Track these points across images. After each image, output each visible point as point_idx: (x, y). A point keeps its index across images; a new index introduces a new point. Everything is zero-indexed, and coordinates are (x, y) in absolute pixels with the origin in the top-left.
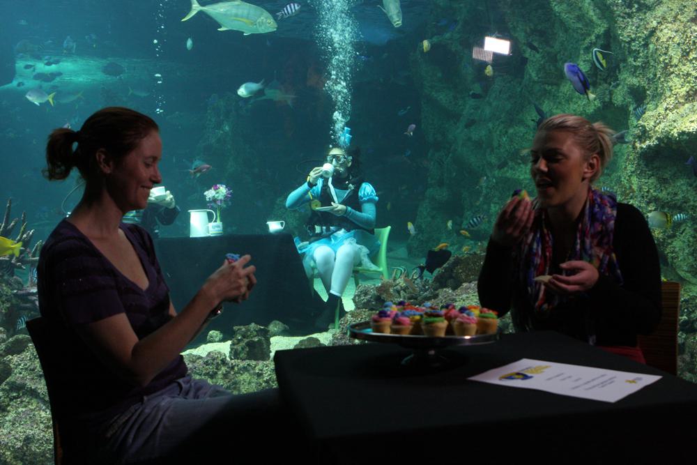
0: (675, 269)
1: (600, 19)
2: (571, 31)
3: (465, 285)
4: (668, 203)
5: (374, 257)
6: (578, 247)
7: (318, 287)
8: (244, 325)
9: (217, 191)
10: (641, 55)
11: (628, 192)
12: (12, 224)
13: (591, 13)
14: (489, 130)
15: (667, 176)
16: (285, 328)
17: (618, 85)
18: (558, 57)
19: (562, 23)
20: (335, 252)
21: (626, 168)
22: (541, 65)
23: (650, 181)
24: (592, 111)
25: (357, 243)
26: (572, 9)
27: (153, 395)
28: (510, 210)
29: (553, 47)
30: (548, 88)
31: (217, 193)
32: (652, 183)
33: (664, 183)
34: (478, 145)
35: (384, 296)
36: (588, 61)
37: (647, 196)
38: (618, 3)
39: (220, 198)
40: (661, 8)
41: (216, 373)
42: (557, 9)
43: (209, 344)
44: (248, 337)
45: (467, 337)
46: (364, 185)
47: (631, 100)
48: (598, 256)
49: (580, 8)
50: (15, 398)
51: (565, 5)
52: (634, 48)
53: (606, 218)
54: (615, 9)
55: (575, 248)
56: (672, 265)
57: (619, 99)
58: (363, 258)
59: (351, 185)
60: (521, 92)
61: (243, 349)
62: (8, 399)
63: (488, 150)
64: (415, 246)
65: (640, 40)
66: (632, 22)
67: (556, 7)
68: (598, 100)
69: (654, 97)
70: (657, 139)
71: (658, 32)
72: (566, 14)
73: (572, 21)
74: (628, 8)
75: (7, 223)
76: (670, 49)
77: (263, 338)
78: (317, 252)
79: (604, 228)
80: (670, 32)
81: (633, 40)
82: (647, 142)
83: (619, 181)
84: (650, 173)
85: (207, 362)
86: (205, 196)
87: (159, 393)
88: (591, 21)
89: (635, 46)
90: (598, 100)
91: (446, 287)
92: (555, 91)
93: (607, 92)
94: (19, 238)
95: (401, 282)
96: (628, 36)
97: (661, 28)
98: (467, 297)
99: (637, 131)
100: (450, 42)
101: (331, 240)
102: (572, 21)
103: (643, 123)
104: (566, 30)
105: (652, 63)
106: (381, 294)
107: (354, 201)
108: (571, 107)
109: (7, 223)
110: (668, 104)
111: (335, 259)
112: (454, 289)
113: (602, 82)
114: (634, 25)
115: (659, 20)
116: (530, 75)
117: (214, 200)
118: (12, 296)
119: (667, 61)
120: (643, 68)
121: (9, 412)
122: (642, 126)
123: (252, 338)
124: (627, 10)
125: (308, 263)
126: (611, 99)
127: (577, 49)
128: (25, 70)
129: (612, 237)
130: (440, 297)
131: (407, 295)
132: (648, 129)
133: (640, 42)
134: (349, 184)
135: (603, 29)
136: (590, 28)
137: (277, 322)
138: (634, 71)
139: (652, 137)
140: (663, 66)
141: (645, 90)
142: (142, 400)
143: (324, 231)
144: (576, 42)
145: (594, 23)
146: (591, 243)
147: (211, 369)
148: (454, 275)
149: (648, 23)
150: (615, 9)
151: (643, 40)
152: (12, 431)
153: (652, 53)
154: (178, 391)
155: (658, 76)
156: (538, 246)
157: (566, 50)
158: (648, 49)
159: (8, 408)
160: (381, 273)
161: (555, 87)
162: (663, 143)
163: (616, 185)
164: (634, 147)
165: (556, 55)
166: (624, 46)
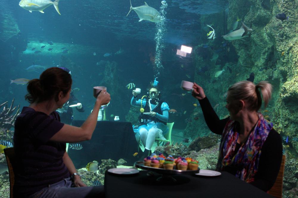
0: (295, 150)
1: (270, 41)
2: (258, 45)
3: (202, 150)
4: (294, 121)
5: (165, 135)
6: (247, 143)
10: (286, 57)
11: (277, 115)
12: (14, 109)
13: (266, 39)
14: (221, 85)
15: (294, 109)
16: (125, 162)
17: (276, 69)
18: (252, 56)
19: (254, 42)
21: (277, 105)
22: (245, 59)
23: (287, 111)
26: (259, 36)
27: (53, 185)
28: (31, 102)
29: (250, 52)
32: (287, 112)
33: (292, 113)
34: (217, 91)
35: (167, 152)
36: (264, 59)
37: (285, 118)
40: (295, 38)
41: (91, 179)
44: (107, 165)
45: (180, 171)
46: (163, 103)
47: (281, 76)
49: (262, 36)
50: (5, 182)
51: (256, 35)
54: (276, 37)
56: (294, 148)
58: (160, 134)
59: (157, 102)
60: (236, 69)
61: (104, 169)
62: (3, 182)
63: (220, 94)
64: (188, 132)
65: (286, 51)
66: (283, 43)
69: (290, 75)
70: (290, 93)
71: (293, 48)
72: (256, 38)
73: (259, 41)
75: (12, 108)
77: (113, 166)
78: (142, 130)
81: (283, 51)
82: (286, 95)
83: (274, 110)
84: (287, 108)
85: (88, 174)
87: (55, 184)
88: (266, 42)
91: (194, 150)
93: (271, 72)
94: (16, 115)
95: (176, 147)
96: (281, 49)
97: (294, 47)
98: (202, 155)
99: (282, 90)
101: (147, 126)
102: (259, 41)
103: (284, 86)
104: (256, 45)
106: (166, 151)
107: (159, 110)
109: (12, 108)
110: (295, 79)
111: (148, 134)
112: (197, 151)
113: (269, 68)
116: (240, 63)
118: (11, 139)
119: (296, 61)
120: (287, 63)
121: (2, 187)
122: (284, 87)
123: (109, 165)
124: (281, 38)
125: (137, 137)
130: (191, 154)
131: (177, 152)
132: (286, 89)
133: (286, 52)
134: (156, 102)
135: (271, 46)
136: (265, 45)
137: (122, 159)
138: (283, 64)
140: (294, 62)
141: (287, 73)
142: (48, 186)
143: (145, 121)
144: (260, 50)
145: (267, 42)
146: (253, 143)
147: (90, 177)
148: (198, 145)
150: (276, 37)
152: (2, 195)
153: (291, 57)
154: (64, 184)
155: (292, 67)
157: (256, 53)
159: (2, 186)
161: (250, 69)
162: (293, 95)
163: (273, 112)
164: (280, 96)
165: (251, 55)
166: (279, 53)
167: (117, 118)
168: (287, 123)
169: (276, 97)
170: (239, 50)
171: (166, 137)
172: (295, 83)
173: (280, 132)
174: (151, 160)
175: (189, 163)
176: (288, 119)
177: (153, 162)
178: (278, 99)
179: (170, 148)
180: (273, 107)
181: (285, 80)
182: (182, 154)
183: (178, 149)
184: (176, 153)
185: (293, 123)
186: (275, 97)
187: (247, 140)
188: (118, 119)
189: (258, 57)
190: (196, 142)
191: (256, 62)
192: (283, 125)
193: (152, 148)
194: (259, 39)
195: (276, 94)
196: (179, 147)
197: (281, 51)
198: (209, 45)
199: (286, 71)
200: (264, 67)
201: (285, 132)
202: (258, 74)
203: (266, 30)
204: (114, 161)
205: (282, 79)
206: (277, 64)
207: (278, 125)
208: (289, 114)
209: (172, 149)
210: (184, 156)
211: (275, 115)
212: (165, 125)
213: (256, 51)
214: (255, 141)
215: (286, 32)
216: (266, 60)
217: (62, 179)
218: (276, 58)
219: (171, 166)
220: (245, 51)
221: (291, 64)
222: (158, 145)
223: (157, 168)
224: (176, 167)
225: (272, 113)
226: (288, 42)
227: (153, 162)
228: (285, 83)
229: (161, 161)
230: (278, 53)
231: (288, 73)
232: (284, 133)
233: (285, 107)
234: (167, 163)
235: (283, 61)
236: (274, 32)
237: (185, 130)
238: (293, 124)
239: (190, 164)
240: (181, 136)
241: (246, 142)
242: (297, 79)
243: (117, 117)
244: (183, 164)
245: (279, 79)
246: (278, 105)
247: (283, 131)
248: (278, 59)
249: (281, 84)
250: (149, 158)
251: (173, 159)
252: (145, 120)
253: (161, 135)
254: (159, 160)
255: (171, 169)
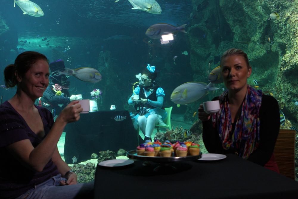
2: (253, 20)
4: (296, 95)
5: (165, 120)
6: (242, 114)
7: (141, 134)
8: (104, 151)
9: (96, 92)
10: (283, 29)
13: (261, 12)
17: (274, 43)
19: (249, 16)
20: (147, 118)
24: (262, 55)
25: (156, 113)
26: (253, 10)
27: (39, 185)
29: (245, 27)
30: (244, 45)
31: (96, 92)
32: (289, 86)
33: (294, 86)
37: (287, 92)
38: (272, 6)
39: (97, 95)
41: (90, 173)
42: (246, 10)
43: (91, 160)
44: (105, 156)
46: (159, 89)
47: (279, 49)
48: (251, 119)
49: (257, 10)
51: (250, 9)
52: (280, 26)
53: (256, 101)
54: (271, 9)
55: (241, 115)
57: (274, 49)
58: (159, 120)
64: (188, 116)
67: (246, 10)
68: (265, 50)
74: (277, 8)
76: (296, 26)
77: (113, 157)
78: (140, 118)
79: (254, 105)
80: (296, 18)
81: (280, 22)
82: (286, 68)
83: (275, 86)
84: (288, 81)
85: (86, 168)
86: (91, 94)
87: (41, 184)
88: (261, 15)
89: (280, 25)
90: (265, 50)
92: (247, 46)
93: (269, 46)
95: (176, 132)
99: (282, 63)
100: (202, 27)
104: (251, 19)
105: (288, 32)
106: (166, 137)
108: (254, 54)
110: (295, 50)
111: (147, 121)
113: (266, 42)
114: (280, 16)
115: (291, 13)
117: (95, 96)
119: (294, 31)
120: (285, 35)
122: (284, 60)
123: (107, 157)
124: (277, 9)
125: (135, 124)
126: (271, 49)
127: (256, 28)
128: (21, 42)
129: (258, 111)
130: (192, 138)
131: (178, 137)
133: (283, 23)
134: (150, 89)
136: (261, 18)
137: (122, 149)
139: (289, 65)
140: (293, 33)
141: (285, 45)
142: (34, 187)
144: (256, 25)
146: (248, 113)
147: (88, 171)
148: (199, 128)
149: (286, 15)
150: (271, 9)
151: (284, 23)
156: (223, 114)
157: (251, 28)
158: (287, 26)
160: (168, 128)
161: (246, 45)
162: (294, 67)
163: (274, 88)
164: (281, 70)
166: (276, 25)
167: (113, 107)
168: (289, 97)
169: (276, 71)
170: (234, 26)
171: (166, 122)
172: (295, 55)
173: (283, 107)
174: (144, 148)
175: (189, 148)
176: (290, 93)
177: (146, 150)
178: (278, 74)
179: (171, 133)
180: (273, 83)
181: (284, 53)
182: (183, 139)
183: (179, 134)
184: (177, 139)
185: (296, 97)
186: (275, 72)
187: (241, 111)
188: (114, 108)
189: (255, 31)
190: (196, 125)
191: (252, 37)
192: (286, 100)
193: (152, 135)
194: (253, 13)
195: (276, 69)
196: (179, 132)
197: (278, 22)
198: (202, 25)
199: (285, 43)
200: (261, 41)
201: (288, 107)
202: (255, 50)
203: (261, 3)
204: (112, 152)
205: (281, 52)
206: (274, 37)
207: (280, 101)
208: (291, 87)
209: (172, 134)
210: (185, 141)
211: (276, 90)
212: (164, 110)
213: (251, 26)
214: (249, 109)
215: (282, 2)
216: (263, 34)
217: (48, 178)
218: (273, 30)
219: (168, 153)
220: (240, 27)
221: (290, 35)
222: (158, 131)
223: (153, 156)
224: (175, 154)
225: (272, 89)
226: (285, 12)
227: (146, 150)
228: (285, 56)
229: (156, 148)
230: (275, 25)
231: (287, 46)
232: (288, 108)
233: (286, 81)
234: (164, 150)
235: (281, 33)
236: (269, 3)
237: (185, 114)
238: (296, 97)
239: (191, 148)
240: (182, 120)
241: (241, 113)
242: (297, 50)
243: (113, 106)
244: (182, 149)
245: (278, 52)
246: (279, 80)
247: (286, 106)
248: (275, 32)
249: (281, 57)
250: (142, 146)
251: (171, 144)
252: (141, 108)
253: (161, 121)
254: (154, 147)
255: (169, 156)
